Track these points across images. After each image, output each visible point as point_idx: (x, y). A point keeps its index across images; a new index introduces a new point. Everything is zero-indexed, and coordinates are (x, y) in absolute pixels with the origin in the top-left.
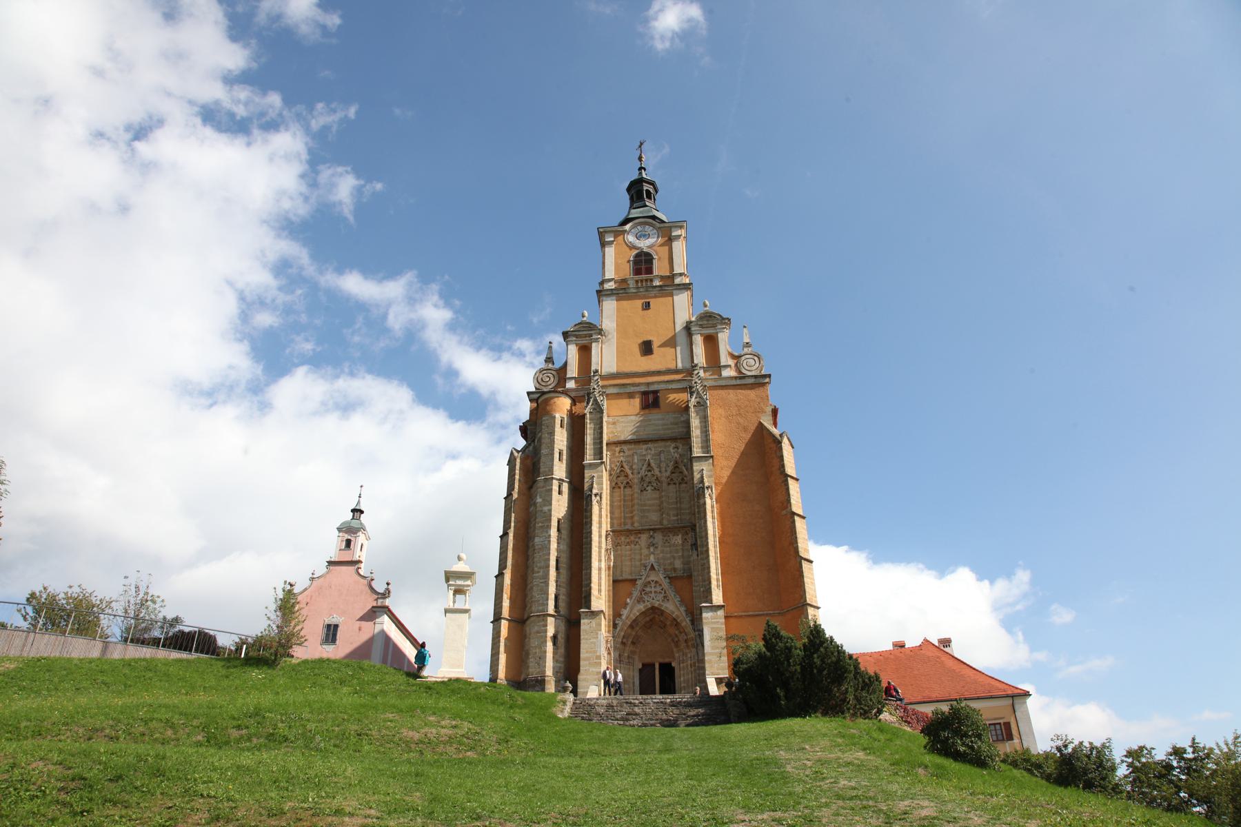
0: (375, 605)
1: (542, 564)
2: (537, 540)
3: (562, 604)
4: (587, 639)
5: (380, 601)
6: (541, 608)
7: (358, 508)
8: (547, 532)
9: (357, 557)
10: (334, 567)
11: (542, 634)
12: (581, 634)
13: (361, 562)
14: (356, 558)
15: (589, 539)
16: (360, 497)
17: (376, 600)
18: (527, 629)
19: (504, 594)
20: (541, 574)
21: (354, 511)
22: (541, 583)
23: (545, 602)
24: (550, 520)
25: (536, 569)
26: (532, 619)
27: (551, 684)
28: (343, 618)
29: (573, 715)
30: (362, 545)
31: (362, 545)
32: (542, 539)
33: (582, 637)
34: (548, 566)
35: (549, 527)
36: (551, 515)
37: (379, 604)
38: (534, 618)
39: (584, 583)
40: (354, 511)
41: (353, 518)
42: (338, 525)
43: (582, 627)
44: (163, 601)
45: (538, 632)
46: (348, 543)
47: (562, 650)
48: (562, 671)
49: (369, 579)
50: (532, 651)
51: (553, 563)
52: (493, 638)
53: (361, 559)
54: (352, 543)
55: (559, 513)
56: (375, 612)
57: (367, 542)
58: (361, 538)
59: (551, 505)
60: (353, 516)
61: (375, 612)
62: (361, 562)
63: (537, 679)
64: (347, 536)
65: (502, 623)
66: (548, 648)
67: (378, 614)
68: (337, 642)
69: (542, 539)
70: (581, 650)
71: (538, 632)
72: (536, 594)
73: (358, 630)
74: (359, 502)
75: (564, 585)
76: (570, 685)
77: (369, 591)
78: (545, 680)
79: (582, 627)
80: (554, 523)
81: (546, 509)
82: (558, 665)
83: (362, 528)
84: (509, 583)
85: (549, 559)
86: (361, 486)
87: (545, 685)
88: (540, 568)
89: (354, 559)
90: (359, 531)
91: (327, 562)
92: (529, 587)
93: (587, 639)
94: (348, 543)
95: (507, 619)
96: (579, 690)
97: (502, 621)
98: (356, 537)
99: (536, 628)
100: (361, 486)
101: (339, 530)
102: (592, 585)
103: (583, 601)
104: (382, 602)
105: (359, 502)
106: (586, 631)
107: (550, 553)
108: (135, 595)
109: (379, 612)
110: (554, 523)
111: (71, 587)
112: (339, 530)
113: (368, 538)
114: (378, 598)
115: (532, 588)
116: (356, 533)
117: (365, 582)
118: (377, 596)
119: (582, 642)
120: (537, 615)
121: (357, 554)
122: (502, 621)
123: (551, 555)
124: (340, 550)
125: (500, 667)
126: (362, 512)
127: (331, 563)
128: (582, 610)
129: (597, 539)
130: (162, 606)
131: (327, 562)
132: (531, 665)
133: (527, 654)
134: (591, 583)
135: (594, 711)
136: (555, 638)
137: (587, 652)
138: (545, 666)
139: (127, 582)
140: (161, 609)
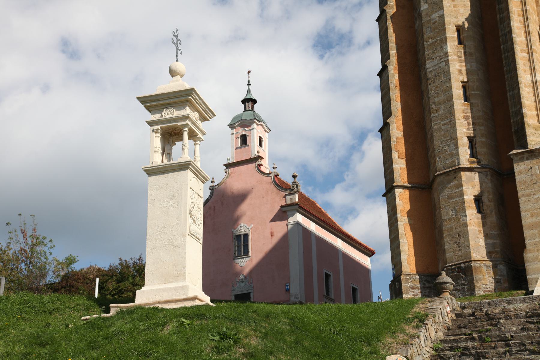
0: (284, 203)
1: (442, 97)
2: (429, 65)
3: (480, 150)
4: (529, 195)
5: (289, 198)
6: (449, 161)
7: (248, 97)
8: (442, 49)
9: (256, 153)
10: (232, 169)
11: (456, 199)
12: (519, 188)
13: (262, 158)
14: (255, 154)
15: (510, 43)
16: (249, 85)
17: (285, 197)
18: (436, 196)
19: (393, 151)
20: (441, 112)
21: (244, 102)
22: (445, 124)
23: (454, 152)
24: (444, 30)
25: (433, 107)
26: (438, 180)
27: (481, 272)
28: (252, 226)
29: (446, 346)
30: (260, 139)
31: (260, 139)
32: (436, 62)
33: (520, 193)
34: (450, 99)
35: (444, 41)
36: (444, 24)
37: (289, 202)
38: (442, 178)
39: (512, 110)
40: (244, 102)
41: (245, 110)
42: (229, 122)
43: (518, 178)
44: (51, 241)
45: (450, 197)
46: (244, 139)
47: (493, 219)
48: (498, 249)
49: (273, 175)
50: (446, 226)
51: (457, 92)
52: (389, 217)
53: (260, 154)
54: (248, 138)
55: (456, 17)
56: (285, 212)
57: (266, 134)
58: (257, 131)
59: (442, 8)
60: (245, 108)
61: (285, 212)
62: (262, 158)
63: (460, 268)
64: (241, 131)
65: (397, 194)
66: (468, 219)
67: (288, 213)
68: (250, 254)
69: (436, 62)
70: (523, 214)
71: (450, 197)
72: (438, 142)
73: (270, 236)
74: (249, 91)
75: (481, 121)
76: (449, 280)
77: (275, 189)
78: (471, 268)
79: (518, 178)
80: (451, 34)
81: (435, 16)
82: (491, 241)
83: (257, 119)
84: (400, 134)
85: (450, 88)
86: (249, 72)
87: (472, 274)
88: (440, 103)
89: (253, 156)
90: (254, 122)
91: (224, 165)
92: (429, 136)
93: (529, 195)
94: (244, 139)
95: (404, 187)
96: (528, 277)
97: (396, 190)
98: (250, 130)
99: (446, 192)
100: (249, 72)
101: (231, 126)
102: (524, 110)
103: (515, 139)
104: (291, 199)
105: (249, 91)
106: (525, 182)
107: (450, 79)
108: (24, 241)
109: (289, 210)
110: (451, 34)
111: (51, 241)
112: (231, 126)
113: (268, 130)
114: (286, 195)
115: (432, 135)
116: (250, 126)
117: (269, 179)
118: (284, 194)
119: (523, 201)
120: (445, 173)
121: (255, 149)
122: (396, 190)
123: (453, 80)
124: (236, 149)
125: (402, 257)
126: (254, 101)
127: (228, 166)
128: (514, 152)
129: (523, 39)
130: (51, 247)
131: (224, 165)
132: (447, 247)
133: (441, 232)
134: (521, 107)
135: (494, 332)
136: (478, 200)
137: (532, 216)
138: (469, 247)
139: (10, 228)
140: (51, 250)
